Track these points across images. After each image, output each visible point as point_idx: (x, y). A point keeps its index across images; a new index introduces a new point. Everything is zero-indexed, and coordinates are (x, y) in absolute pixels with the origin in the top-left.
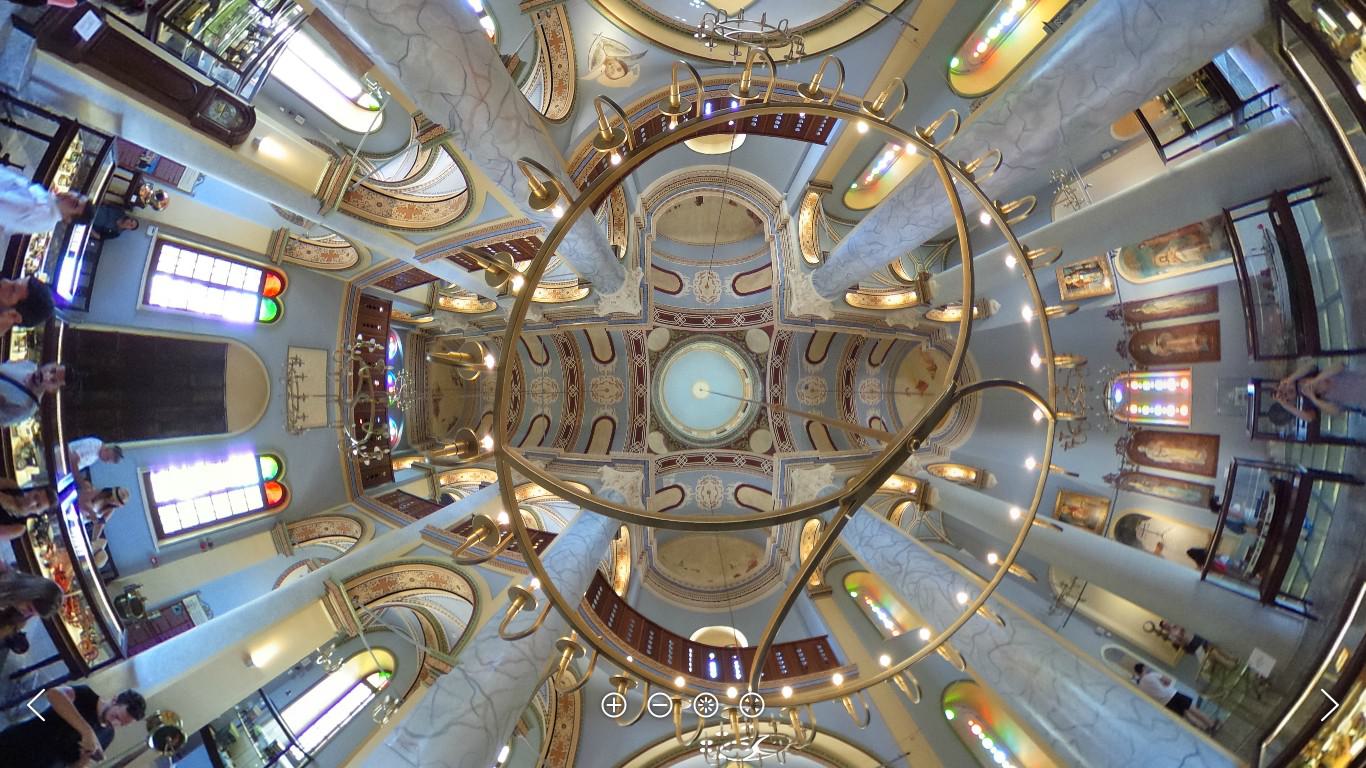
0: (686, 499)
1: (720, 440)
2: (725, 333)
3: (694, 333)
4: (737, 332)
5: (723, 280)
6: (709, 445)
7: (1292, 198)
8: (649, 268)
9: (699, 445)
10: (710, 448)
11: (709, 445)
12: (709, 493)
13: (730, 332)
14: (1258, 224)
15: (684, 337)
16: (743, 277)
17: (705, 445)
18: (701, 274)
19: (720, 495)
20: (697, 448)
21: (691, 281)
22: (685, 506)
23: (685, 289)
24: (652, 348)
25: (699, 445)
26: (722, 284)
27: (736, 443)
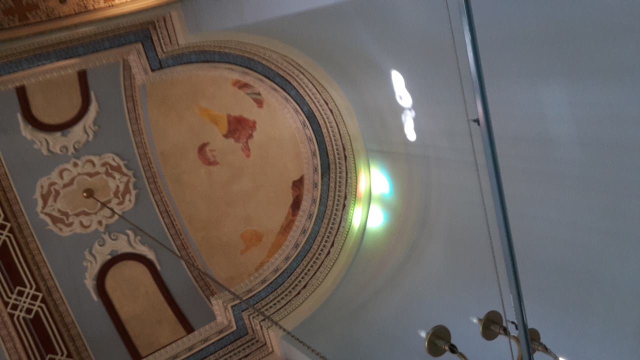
26: (108, 229)
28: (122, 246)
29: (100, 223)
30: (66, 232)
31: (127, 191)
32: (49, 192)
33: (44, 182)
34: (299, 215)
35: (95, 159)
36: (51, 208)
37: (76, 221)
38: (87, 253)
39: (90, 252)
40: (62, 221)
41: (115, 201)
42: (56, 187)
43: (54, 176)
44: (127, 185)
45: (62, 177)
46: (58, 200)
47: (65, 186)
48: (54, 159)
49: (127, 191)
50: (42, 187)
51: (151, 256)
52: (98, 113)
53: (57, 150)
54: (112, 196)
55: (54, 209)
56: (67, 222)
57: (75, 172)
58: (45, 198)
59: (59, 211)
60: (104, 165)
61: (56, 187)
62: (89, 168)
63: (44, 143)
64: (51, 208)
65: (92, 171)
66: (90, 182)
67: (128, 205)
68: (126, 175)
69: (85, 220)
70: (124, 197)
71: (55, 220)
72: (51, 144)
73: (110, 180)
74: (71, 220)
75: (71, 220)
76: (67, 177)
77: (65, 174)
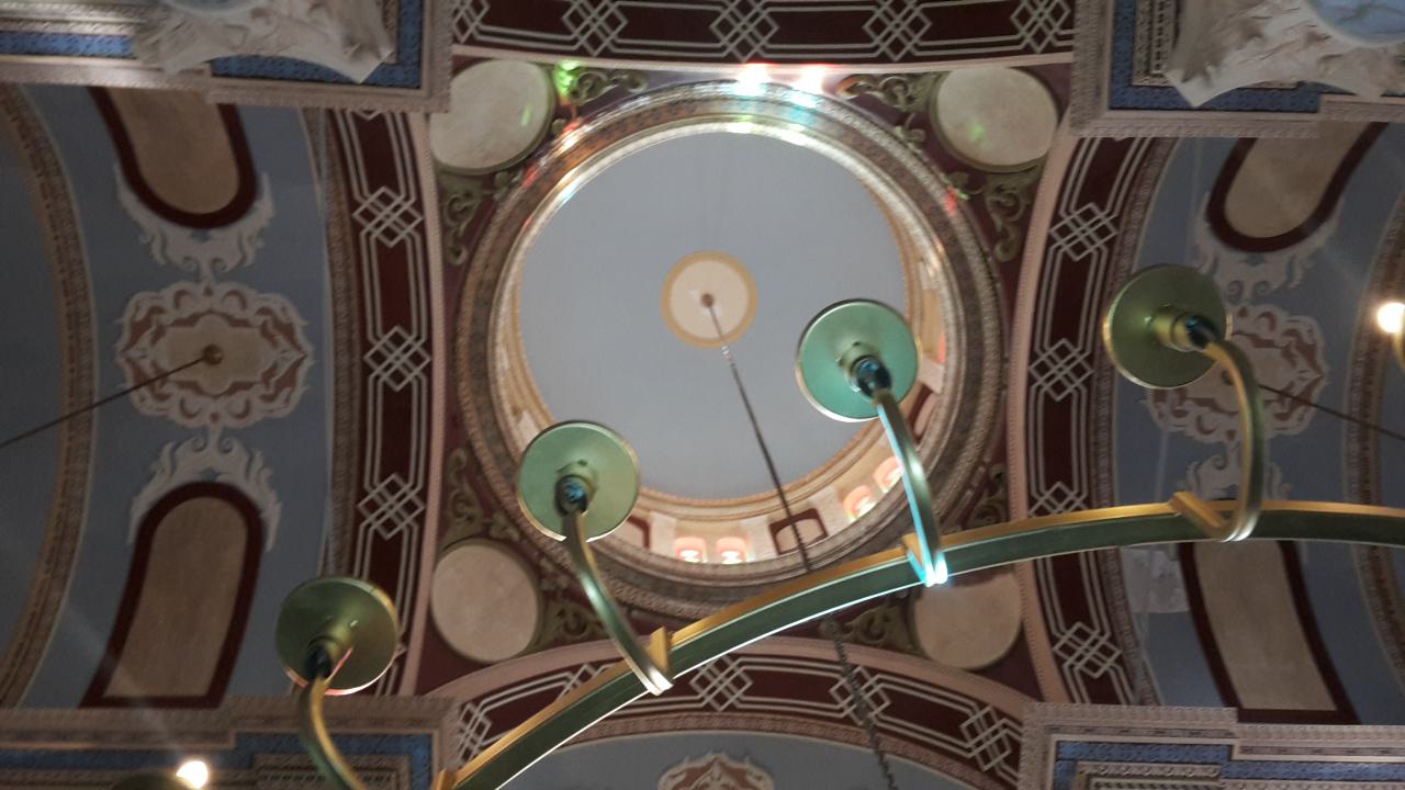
0: (178, 236)
1: (1000, 319)
2: (448, 269)
3: (455, 421)
4: (449, 212)
5: (171, 273)
6: (990, 356)
7: (803, 571)
8: (1232, 127)
9: (985, 406)
10: (1004, 360)
11: (990, 356)
12: (210, 356)
13: (450, 251)
14: (712, 291)
15: (474, 469)
16: (147, 171)
17: (990, 373)
18: (1308, 352)
19: (205, 406)
20: (1000, 406)
21: (183, 435)
22: (137, 228)
23: (231, 468)
24: (523, 639)
25: (985, 406)
26: (196, 277)
27: (992, 235)
28: (179, 239)
29: (209, 292)
30: (276, 302)
31: (138, 329)
32: (279, 387)
33: (281, 409)
34: (1022, 758)
35: (250, 294)
36: (1304, 375)
37: (250, 314)
38: (250, 260)
39: (244, 259)
40: (278, 325)
41: (261, 390)
42: (263, 391)
43: (259, 411)
44: (133, 342)
45: (177, 304)
46: (269, 365)
47: (179, 323)
48: (171, 273)
49: (138, 329)
50: (287, 400)
51: (128, 198)
52: (137, 491)
53: (237, 447)
54: (258, 378)
55: (284, 351)
56: (157, 391)
57: (203, 304)
58: (289, 379)
59: (275, 344)
60: (163, 398)
61: (263, 391)
62: (194, 402)
63: (253, 474)
64: (1304, 375)
65: (239, 314)
66: (225, 336)
67: (140, 304)
68: (129, 360)
69: (232, 306)
70: (279, 388)
71: (288, 331)
72: (242, 467)
73: (265, 344)
74: (261, 319)
75: (261, 319)
76: (238, 402)
77: (240, 409)
